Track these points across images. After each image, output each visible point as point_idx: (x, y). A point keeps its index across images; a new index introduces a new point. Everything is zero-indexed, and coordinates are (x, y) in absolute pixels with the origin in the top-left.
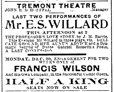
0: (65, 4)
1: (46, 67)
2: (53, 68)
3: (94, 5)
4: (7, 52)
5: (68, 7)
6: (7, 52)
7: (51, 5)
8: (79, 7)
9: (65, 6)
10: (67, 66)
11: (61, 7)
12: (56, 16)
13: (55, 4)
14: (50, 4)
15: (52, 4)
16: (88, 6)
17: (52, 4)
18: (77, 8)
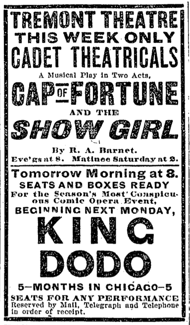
0: (70, 284)
1: (112, 286)
2: (51, 37)
3: (115, 184)
4: (42, 77)
5: (120, 290)
6: (42, 77)
7: (60, 285)
8: (162, 213)
9: (70, 287)
10: (71, 34)
11: (15, 176)
12: (136, 184)
13: (114, 208)
14: (58, 284)
15: (61, 284)
16: (134, 186)
17: (61, 284)
18: (149, 188)
